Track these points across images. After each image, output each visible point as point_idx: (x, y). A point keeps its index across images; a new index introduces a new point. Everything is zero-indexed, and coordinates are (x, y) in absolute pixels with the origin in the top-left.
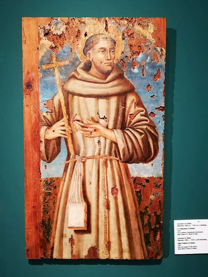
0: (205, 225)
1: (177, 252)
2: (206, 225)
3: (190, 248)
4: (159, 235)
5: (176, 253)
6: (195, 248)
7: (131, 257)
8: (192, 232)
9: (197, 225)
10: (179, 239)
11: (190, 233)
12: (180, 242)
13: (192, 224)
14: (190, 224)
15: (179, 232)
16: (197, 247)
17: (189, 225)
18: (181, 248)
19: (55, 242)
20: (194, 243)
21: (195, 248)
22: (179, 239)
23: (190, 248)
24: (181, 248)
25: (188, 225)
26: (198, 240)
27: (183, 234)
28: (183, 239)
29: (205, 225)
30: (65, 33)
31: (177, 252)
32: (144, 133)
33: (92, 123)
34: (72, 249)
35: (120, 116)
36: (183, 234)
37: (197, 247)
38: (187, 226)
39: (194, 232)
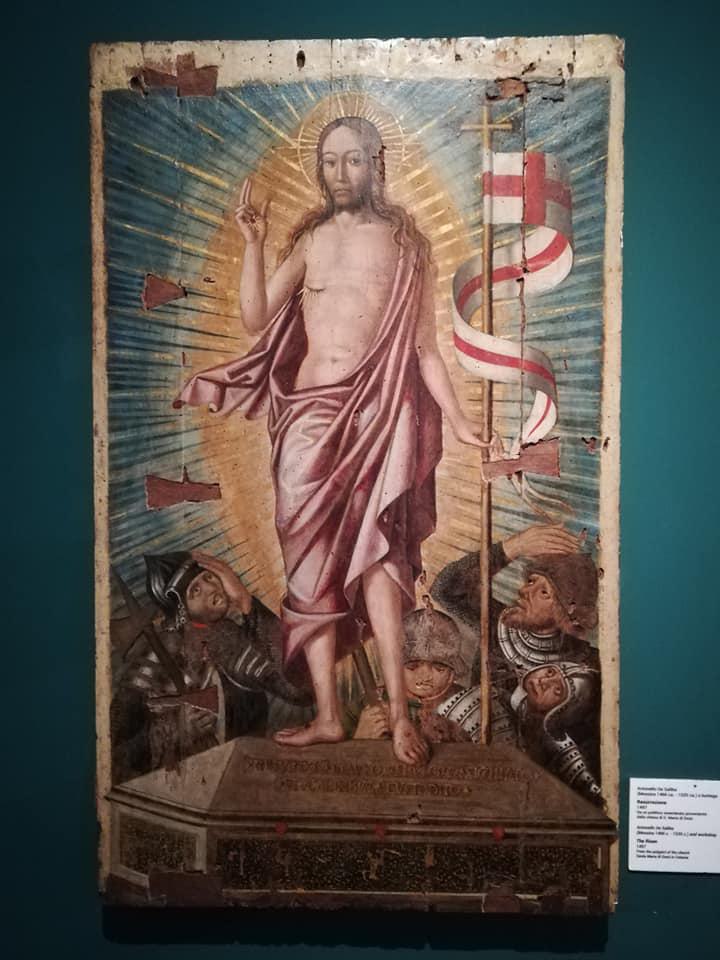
0: (710, 835)
2: (715, 797)
3: (671, 854)
5: (631, 868)
6: (683, 855)
8: (676, 813)
9: (693, 796)
10: (641, 830)
12: (643, 837)
13: (675, 830)
14: (675, 790)
16: (688, 853)
17: (671, 792)
18: (646, 854)
19: (549, 287)
23: (671, 854)
25: (667, 792)
26: (691, 835)
27: (653, 815)
28: (653, 792)
29: (710, 835)
32: (352, 605)
33: (527, 74)
36: (653, 815)
37: (688, 853)
38: (665, 795)
39: (681, 814)
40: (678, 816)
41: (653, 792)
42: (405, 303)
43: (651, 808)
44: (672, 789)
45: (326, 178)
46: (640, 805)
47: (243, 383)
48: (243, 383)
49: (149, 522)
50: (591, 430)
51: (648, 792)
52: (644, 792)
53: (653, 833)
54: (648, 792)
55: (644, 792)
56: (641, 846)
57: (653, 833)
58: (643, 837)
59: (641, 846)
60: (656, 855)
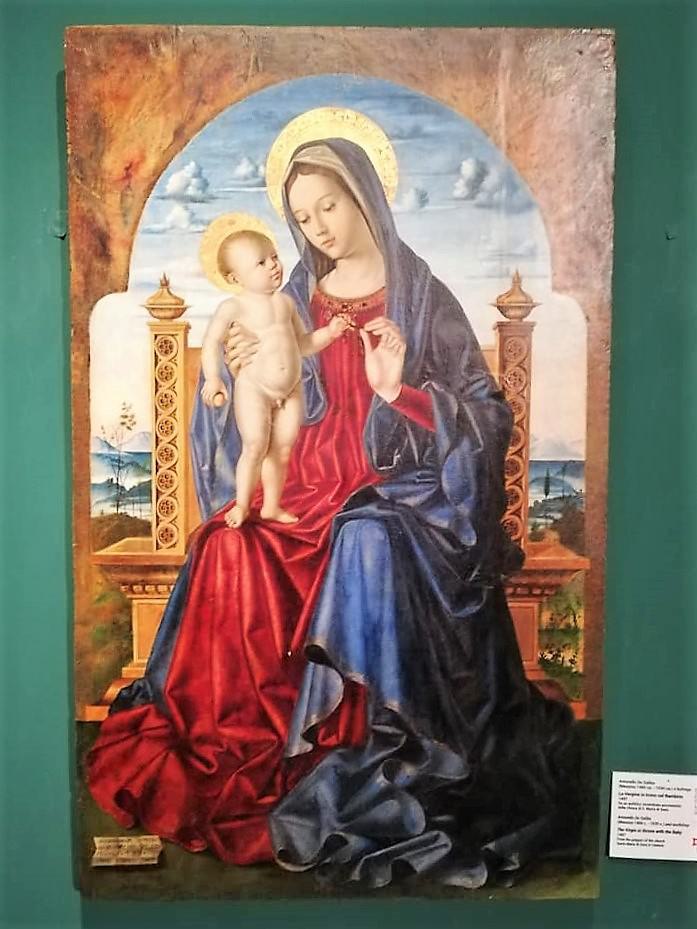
1: (616, 851)
3: (648, 842)
4: (180, 27)
5: (614, 773)
7: (94, 485)
11: (650, 807)
12: (622, 826)
13: (652, 820)
15: (623, 801)
17: (649, 785)
18: (626, 842)
20: (679, 806)
21: (659, 844)
22: (622, 784)
23: (648, 842)
24: (626, 842)
28: (631, 820)
30: (351, 532)
31: (616, 851)
34: (163, 649)
35: (429, 571)
36: (632, 806)
40: (656, 808)
41: (631, 820)
42: (336, 537)
43: (630, 799)
44: (650, 783)
45: (301, 413)
46: (621, 832)
47: (431, 530)
48: (431, 530)
49: (366, 706)
50: (560, 488)
51: (629, 784)
52: (625, 784)
53: (634, 787)
54: (629, 784)
55: (625, 784)
56: (621, 835)
57: (634, 787)
58: (622, 826)
59: (621, 835)
60: (635, 842)
